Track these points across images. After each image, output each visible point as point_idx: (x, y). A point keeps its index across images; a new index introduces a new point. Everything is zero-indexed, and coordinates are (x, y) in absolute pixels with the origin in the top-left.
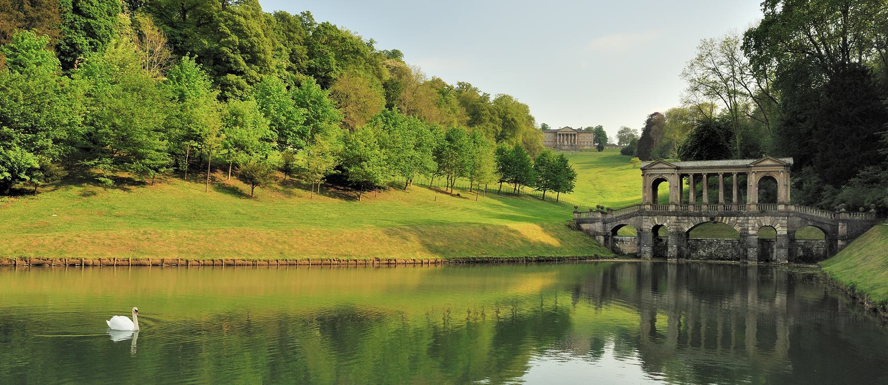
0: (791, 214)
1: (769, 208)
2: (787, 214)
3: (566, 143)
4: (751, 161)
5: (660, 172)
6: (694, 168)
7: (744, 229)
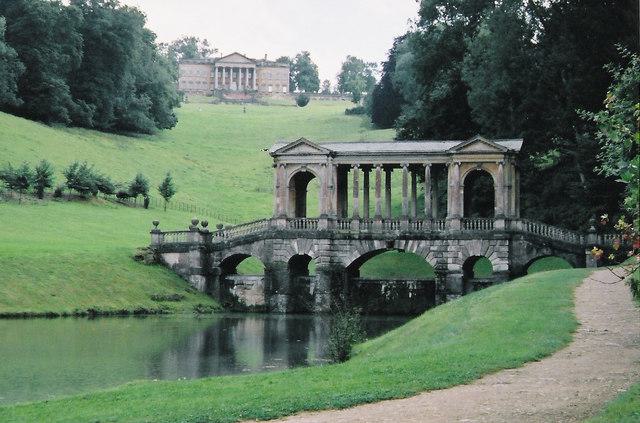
1: (477, 221)
2: (511, 235)
3: (233, 86)
4: (457, 143)
5: (303, 160)
6: (433, 154)
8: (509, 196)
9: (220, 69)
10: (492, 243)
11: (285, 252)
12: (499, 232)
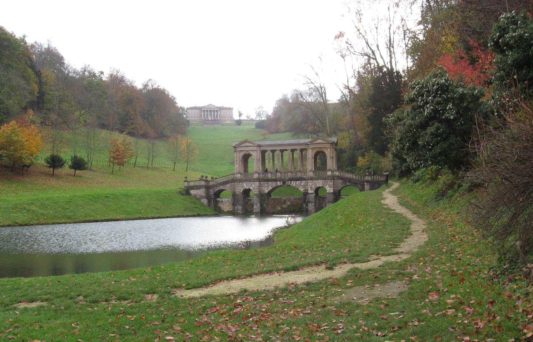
0: (335, 178)
1: (322, 173)
2: (333, 178)
7: (306, 190)
8: (333, 161)
9: (204, 111)
10: (327, 181)
11: (240, 188)
12: (329, 176)
